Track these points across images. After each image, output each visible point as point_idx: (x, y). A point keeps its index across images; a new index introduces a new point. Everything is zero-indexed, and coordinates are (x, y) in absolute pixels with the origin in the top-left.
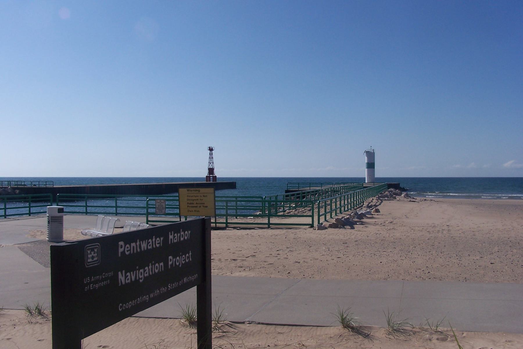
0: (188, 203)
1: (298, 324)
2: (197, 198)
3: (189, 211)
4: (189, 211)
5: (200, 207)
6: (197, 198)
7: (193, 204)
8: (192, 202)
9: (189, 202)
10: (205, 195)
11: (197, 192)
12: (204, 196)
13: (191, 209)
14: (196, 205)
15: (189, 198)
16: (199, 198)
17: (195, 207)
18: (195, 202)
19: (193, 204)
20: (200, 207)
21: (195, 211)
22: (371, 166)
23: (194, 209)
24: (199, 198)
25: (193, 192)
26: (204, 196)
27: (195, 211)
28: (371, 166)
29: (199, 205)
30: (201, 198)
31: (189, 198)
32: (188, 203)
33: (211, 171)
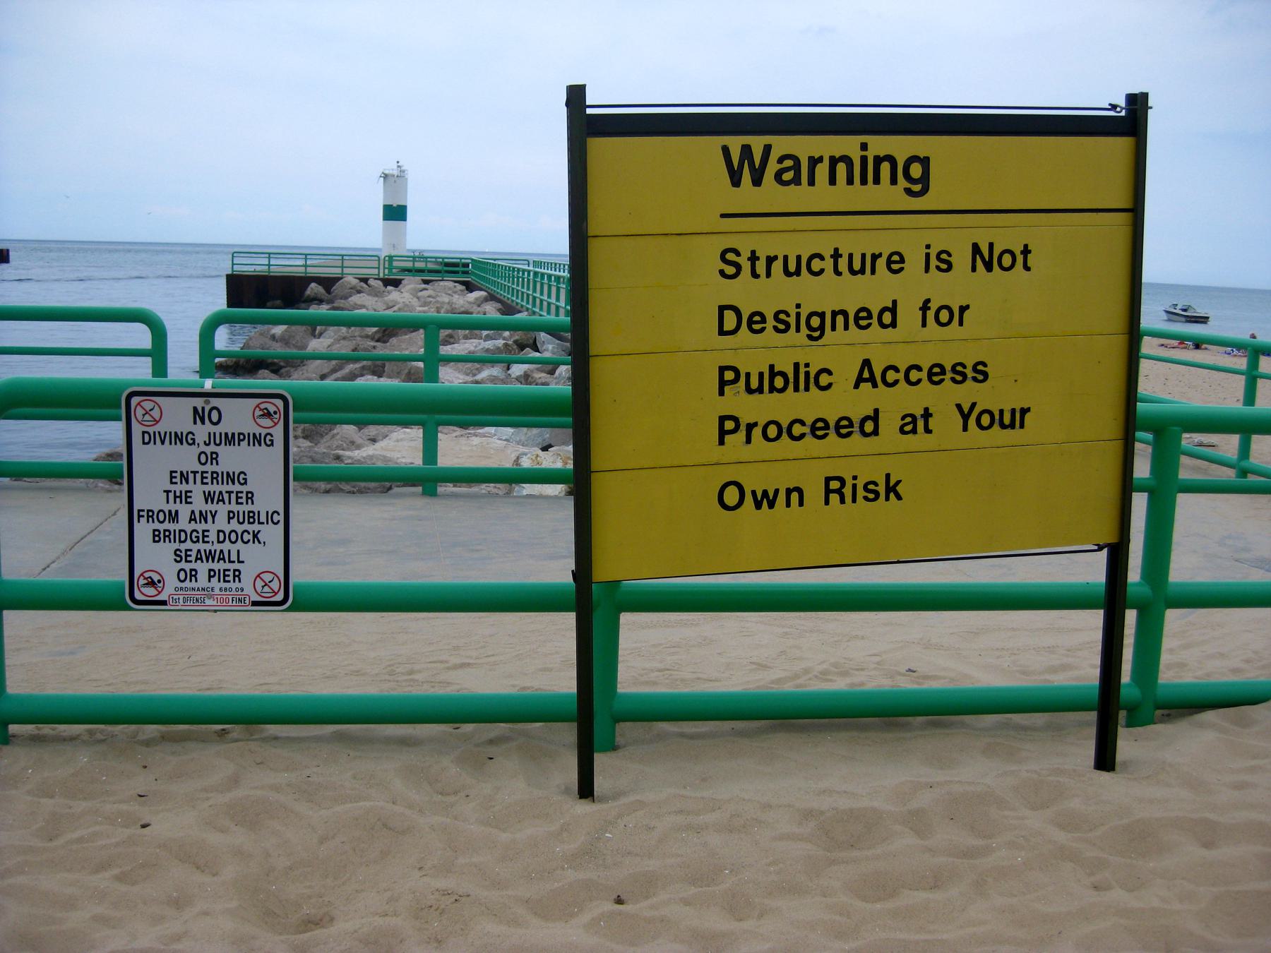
0: (727, 377)
1: (812, 234)
2: (874, 291)
3: (733, 495)
4: (733, 495)
5: (913, 423)
6: (874, 291)
7: (805, 379)
8: (786, 350)
9: (753, 351)
10: (1006, 235)
11: (889, 194)
12: (984, 258)
13: (763, 465)
14: (859, 403)
15: (753, 351)
16: (911, 288)
17: (843, 428)
18: (841, 352)
19: (805, 379)
20: (913, 423)
21: (834, 488)
22: (395, 213)
23: (808, 463)
24: (911, 288)
25: (821, 195)
26: (984, 258)
27: (834, 488)
28: (395, 213)
29: (895, 402)
30: (943, 289)
31: (749, 294)
32: (727, 377)
33: (14, 736)
